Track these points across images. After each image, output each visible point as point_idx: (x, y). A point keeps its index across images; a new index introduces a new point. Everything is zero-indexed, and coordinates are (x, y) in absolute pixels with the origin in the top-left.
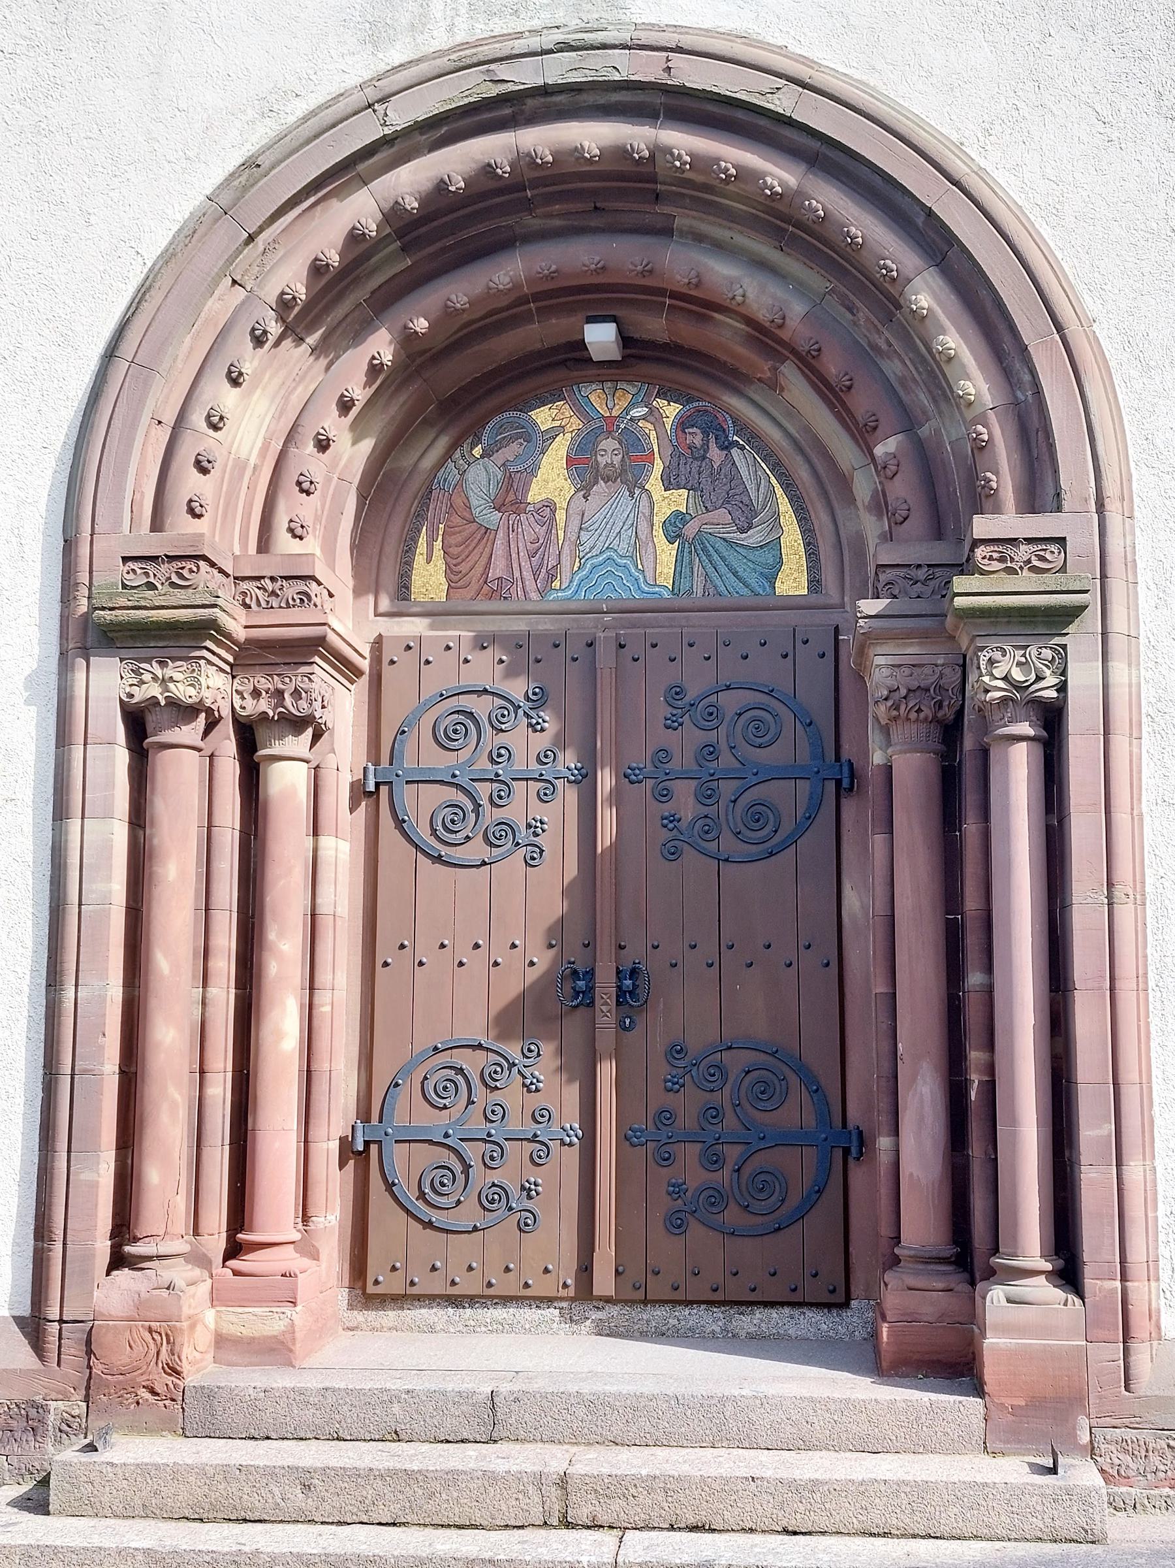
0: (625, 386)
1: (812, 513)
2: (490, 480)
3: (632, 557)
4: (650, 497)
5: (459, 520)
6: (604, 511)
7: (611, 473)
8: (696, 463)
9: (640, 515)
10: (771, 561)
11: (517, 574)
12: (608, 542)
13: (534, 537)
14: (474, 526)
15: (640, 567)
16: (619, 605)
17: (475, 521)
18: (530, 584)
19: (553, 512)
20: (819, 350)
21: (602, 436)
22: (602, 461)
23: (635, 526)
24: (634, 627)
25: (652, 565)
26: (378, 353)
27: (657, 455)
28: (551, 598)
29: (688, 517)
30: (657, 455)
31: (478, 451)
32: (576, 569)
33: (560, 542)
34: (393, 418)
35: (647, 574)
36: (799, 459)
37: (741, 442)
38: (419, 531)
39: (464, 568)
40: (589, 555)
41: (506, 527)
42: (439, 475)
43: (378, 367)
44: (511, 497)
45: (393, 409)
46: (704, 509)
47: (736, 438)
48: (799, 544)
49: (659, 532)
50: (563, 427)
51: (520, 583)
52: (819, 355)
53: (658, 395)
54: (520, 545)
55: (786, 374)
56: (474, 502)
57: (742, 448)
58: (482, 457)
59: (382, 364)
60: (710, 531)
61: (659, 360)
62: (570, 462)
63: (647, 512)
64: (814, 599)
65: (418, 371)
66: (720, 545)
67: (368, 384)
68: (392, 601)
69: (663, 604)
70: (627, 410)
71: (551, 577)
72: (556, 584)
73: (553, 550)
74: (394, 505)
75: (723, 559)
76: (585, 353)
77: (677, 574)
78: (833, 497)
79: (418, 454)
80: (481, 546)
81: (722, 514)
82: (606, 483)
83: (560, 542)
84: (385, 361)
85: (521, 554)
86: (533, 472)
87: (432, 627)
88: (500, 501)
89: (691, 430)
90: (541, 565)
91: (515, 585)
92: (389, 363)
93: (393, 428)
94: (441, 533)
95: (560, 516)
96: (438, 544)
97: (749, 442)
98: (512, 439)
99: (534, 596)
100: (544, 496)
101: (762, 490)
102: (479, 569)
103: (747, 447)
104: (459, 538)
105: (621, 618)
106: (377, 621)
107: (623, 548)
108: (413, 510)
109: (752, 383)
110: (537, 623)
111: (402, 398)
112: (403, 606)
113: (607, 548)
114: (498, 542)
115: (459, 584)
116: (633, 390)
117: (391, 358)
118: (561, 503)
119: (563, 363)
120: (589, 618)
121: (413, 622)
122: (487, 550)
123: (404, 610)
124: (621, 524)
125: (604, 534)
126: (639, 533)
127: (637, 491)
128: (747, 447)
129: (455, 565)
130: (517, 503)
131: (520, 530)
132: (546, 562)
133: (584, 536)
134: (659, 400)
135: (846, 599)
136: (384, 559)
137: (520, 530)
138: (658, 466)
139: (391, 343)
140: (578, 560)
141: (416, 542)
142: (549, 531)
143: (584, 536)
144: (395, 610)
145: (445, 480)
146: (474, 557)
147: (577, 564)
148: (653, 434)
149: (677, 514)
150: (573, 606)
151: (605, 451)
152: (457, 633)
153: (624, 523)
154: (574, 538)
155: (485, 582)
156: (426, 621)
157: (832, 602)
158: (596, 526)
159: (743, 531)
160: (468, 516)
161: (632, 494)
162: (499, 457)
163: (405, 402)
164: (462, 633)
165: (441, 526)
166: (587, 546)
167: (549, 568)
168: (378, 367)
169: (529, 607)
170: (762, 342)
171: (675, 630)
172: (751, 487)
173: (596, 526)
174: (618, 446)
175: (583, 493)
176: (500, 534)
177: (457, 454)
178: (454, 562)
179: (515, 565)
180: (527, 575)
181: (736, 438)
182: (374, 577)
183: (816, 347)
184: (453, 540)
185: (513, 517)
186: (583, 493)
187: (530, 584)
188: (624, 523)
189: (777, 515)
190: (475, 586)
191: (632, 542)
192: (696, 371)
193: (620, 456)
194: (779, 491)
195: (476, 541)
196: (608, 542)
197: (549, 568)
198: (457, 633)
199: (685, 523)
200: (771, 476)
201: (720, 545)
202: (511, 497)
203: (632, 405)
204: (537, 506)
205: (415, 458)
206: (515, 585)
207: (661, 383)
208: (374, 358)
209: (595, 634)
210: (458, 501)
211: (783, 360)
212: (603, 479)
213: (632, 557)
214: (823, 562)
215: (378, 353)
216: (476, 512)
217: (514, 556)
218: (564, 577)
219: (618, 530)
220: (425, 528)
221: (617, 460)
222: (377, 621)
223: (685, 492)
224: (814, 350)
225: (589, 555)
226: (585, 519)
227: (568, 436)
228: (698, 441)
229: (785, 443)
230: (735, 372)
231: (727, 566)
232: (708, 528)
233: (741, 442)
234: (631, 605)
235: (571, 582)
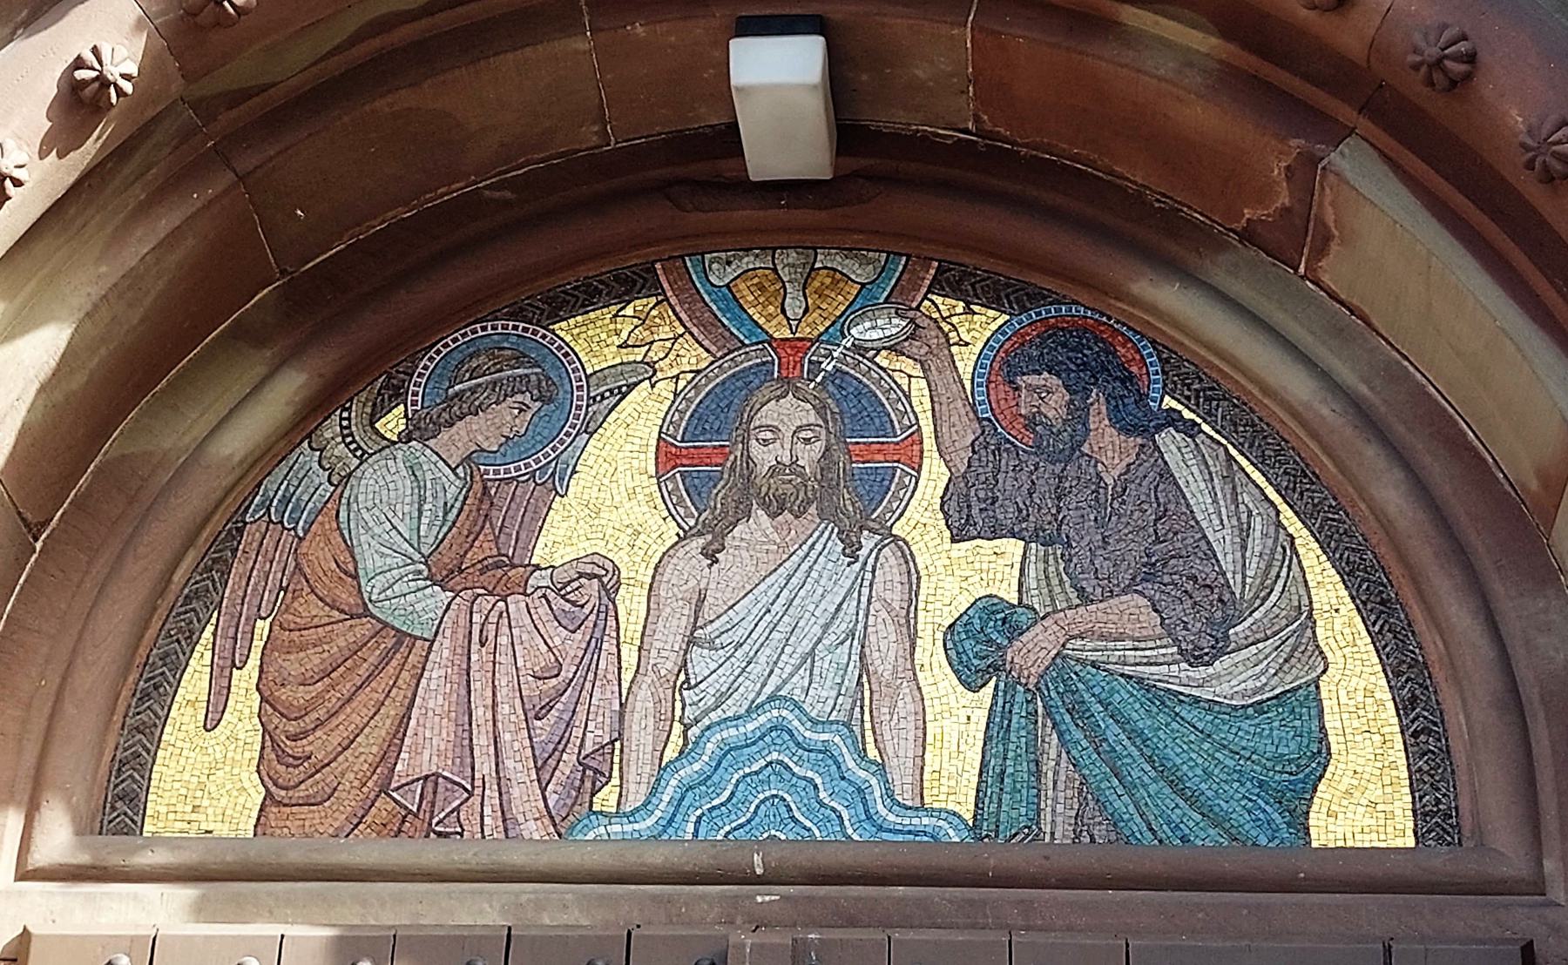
0: (837, 261)
1: (1417, 613)
2: (422, 501)
3: (847, 725)
4: (908, 558)
5: (317, 609)
6: (766, 593)
7: (789, 489)
8: (1048, 470)
9: (876, 605)
10: (1289, 749)
11: (485, 767)
12: (774, 681)
13: (544, 659)
14: (364, 628)
15: (872, 753)
16: (804, 859)
17: (367, 613)
18: (525, 796)
19: (610, 591)
20: (1471, 58)
21: (766, 392)
22: (764, 457)
23: (858, 637)
24: (852, 922)
25: (909, 749)
26: (95, 51)
27: (929, 443)
28: (591, 836)
29: (1023, 617)
30: (929, 443)
31: (393, 423)
32: (670, 754)
33: (627, 677)
34: (132, 281)
35: (895, 775)
36: (1372, 454)
37: (1187, 414)
38: (192, 639)
39: (319, 745)
40: (714, 716)
41: (461, 632)
42: (269, 485)
43: (88, 91)
44: (484, 549)
45: (138, 248)
46: (1074, 595)
47: (1169, 402)
48: (1382, 704)
49: (931, 653)
50: (652, 365)
51: (492, 793)
52: (1468, 77)
53: (937, 286)
54: (502, 681)
55: (1349, 175)
56: (370, 560)
57: (1191, 429)
58: (406, 437)
59: (103, 82)
60: (1093, 656)
61: (946, 187)
62: (668, 456)
63: (896, 597)
64: (1441, 860)
65: (222, 155)
66: (1123, 695)
67: (60, 140)
68: (79, 833)
69: (943, 860)
70: (841, 326)
71: (593, 774)
72: (607, 798)
73: (604, 698)
74: (120, 557)
75: (1134, 734)
76: (732, 163)
77: (991, 777)
78: (1485, 562)
79: (212, 418)
80: (382, 682)
81: (1131, 608)
82: (773, 516)
83: (627, 677)
84: (113, 72)
85: (504, 709)
86: (555, 481)
87: (201, 912)
88: (448, 557)
89: (1033, 379)
90: (561, 745)
91: (476, 800)
92: (128, 87)
93: (136, 316)
94: (258, 644)
95: (631, 604)
96: (245, 679)
97: (1209, 416)
98: (503, 391)
99: (534, 829)
100: (581, 548)
101: (1256, 543)
102: (369, 746)
103: (1205, 428)
104: (314, 660)
105: (810, 899)
106: (20, 894)
107: (822, 698)
108: (179, 577)
109: (1220, 246)
110: (539, 906)
111: (165, 222)
112: (114, 851)
113: (771, 698)
114: (434, 674)
115: (301, 793)
116: (859, 273)
117: (133, 69)
118: (635, 570)
119: (663, 189)
120: (703, 897)
121: (136, 897)
122: (392, 710)
123: (115, 860)
124: (817, 630)
125: (762, 658)
126: (874, 657)
127: (868, 542)
128: (1205, 428)
129: (294, 738)
130: (497, 566)
131: (504, 640)
132: (577, 732)
133: (701, 662)
134: (939, 300)
135: (1549, 865)
136: (69, 709)
137: (504, 640)
138: (934, 475)
139: (139, 26)
140: (677, 728)
141: (179, 668)
142: (594, 646)
143: (701, 662)
144: (84, 858)
145: (286, 500)
146: (355, 715)
147: (676, 741)
148: (919, 388)
149: (989, 607)
150: (656, 857)
151: (773, 429)
152: (275, 930)
153: (826, 627)
154: (669, 665)
155: (384, 789)
156: (185, 893)
157: (1505, 871)
158: (740, 633)
159: (1196, 658)
160: (346, 598)
161: (851, 551)
162: (458, 438)
163: (175, 235)
164: (291, 931)
165: (260, 623)
166: (711, 688)
167: (589, 747)
168: (88, 91)
169: (516, 857)
170: (1268, 87)
171: (991, 936)
172: (1223, 542)
173: (740, 633)
174: (812, 418)
175: (701, 541)
176: (443, 650)
177: (331, 430)
178: (292, 728)
179: (482, 740)
180: (519, 769)
181: (1169, 402)
182: (30, 758)
183: (1462, 47)
184: (292, 665)
185: (485, 603)
186: (701, 541)
187: (525, 796)
188: (826, 627)
189: (1305, 616)
190: (348, 800)
191: (850, 682)
192: (1054, 215)
193: (819, 446)
194: (1310, 553)
195: (363, 671)
196: (774, 681)
197: (589, 747)
198: (275, 930)
199: (1014, 631)
200: (1283, 507)
201: (1123, 695)
202: (484, 549)
203: (862, 306)
204: (561, 576)
205: (200, 430)
206: (476, 800)
207: (953, 255)
208: (79, 63)
209: (726, 937)
210: (320, 555)
211: (1338, 134)
212: (765, 506)
213: (847, 725)
214: (1460, 757)
215: (95, 51)
216: (373, 588)
217: (480, 714)
218: (631, 777)
219: (806, 646)
220: (210, 629)
221: (809, 456)
222: (20, 894)
223: (1013, 547)
224: (1457, 58)
225: (714, 716)
226: (707, 613)
227: (666, 389)
228: (1055, 404)
229: (1327, 411)
230: (1172, 223)
231: (1150, 760)
232: (1087, 649)
233: (1187, 414)
234: (846, 858)
235: (653, 792)
